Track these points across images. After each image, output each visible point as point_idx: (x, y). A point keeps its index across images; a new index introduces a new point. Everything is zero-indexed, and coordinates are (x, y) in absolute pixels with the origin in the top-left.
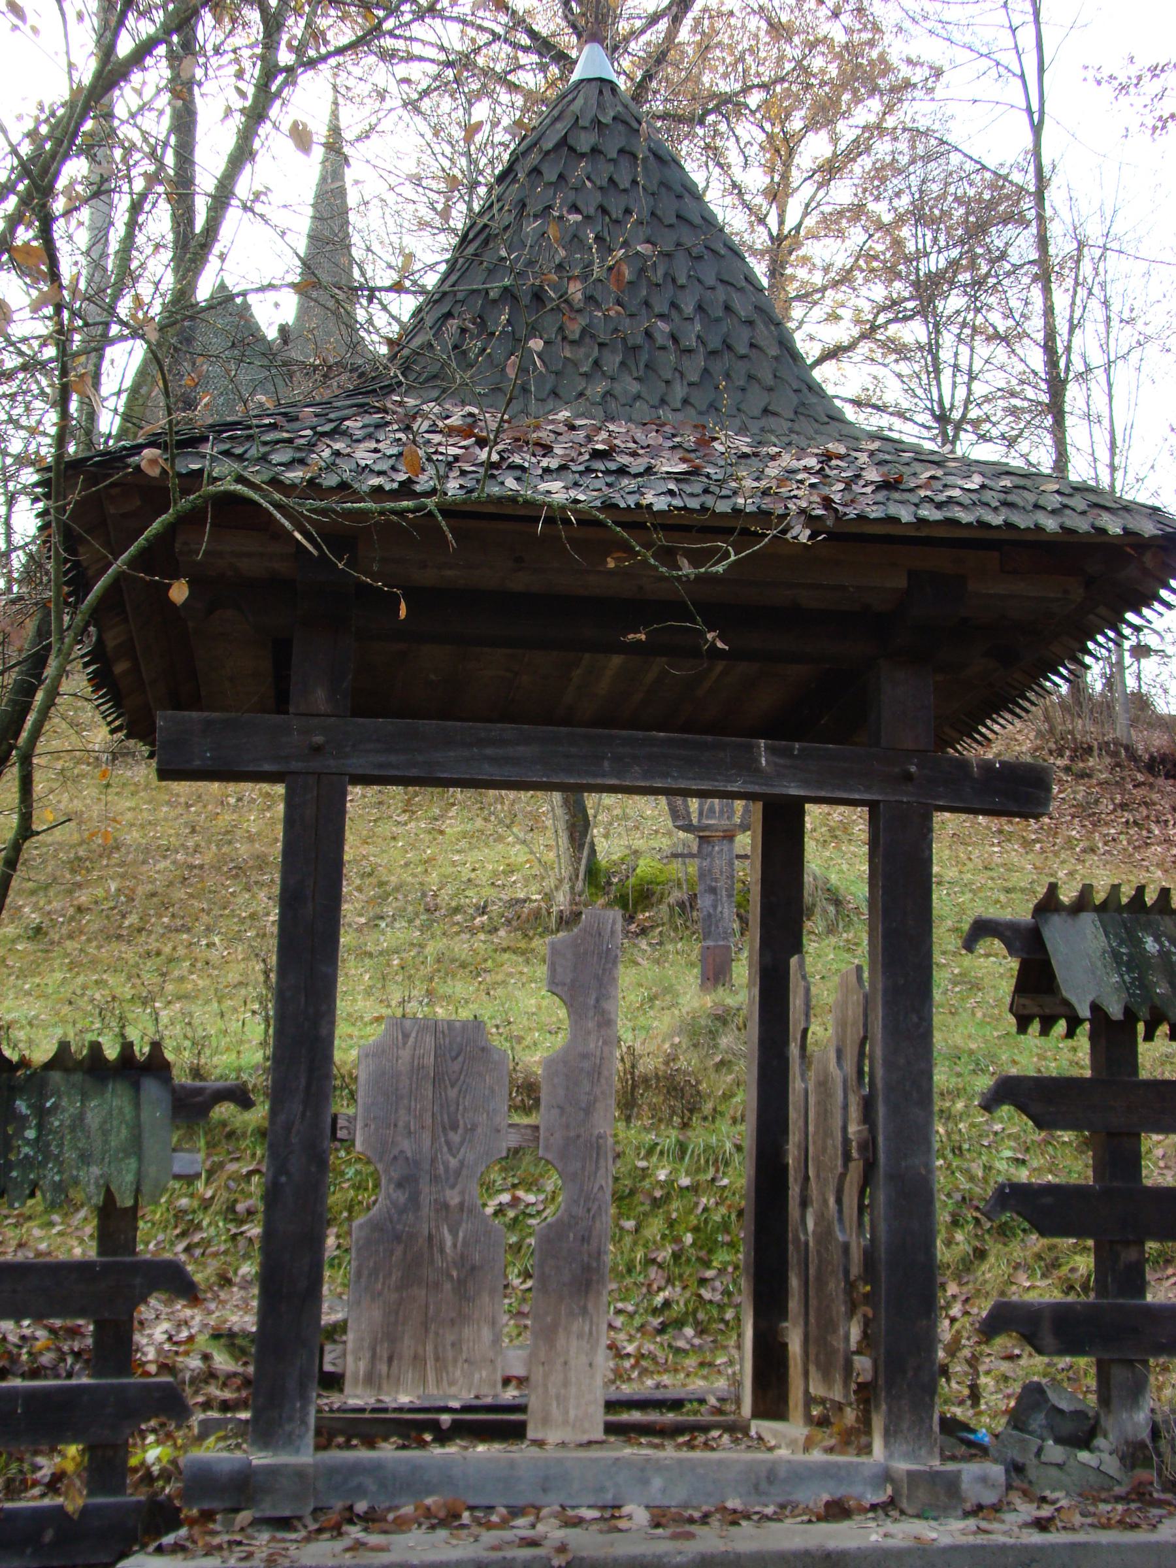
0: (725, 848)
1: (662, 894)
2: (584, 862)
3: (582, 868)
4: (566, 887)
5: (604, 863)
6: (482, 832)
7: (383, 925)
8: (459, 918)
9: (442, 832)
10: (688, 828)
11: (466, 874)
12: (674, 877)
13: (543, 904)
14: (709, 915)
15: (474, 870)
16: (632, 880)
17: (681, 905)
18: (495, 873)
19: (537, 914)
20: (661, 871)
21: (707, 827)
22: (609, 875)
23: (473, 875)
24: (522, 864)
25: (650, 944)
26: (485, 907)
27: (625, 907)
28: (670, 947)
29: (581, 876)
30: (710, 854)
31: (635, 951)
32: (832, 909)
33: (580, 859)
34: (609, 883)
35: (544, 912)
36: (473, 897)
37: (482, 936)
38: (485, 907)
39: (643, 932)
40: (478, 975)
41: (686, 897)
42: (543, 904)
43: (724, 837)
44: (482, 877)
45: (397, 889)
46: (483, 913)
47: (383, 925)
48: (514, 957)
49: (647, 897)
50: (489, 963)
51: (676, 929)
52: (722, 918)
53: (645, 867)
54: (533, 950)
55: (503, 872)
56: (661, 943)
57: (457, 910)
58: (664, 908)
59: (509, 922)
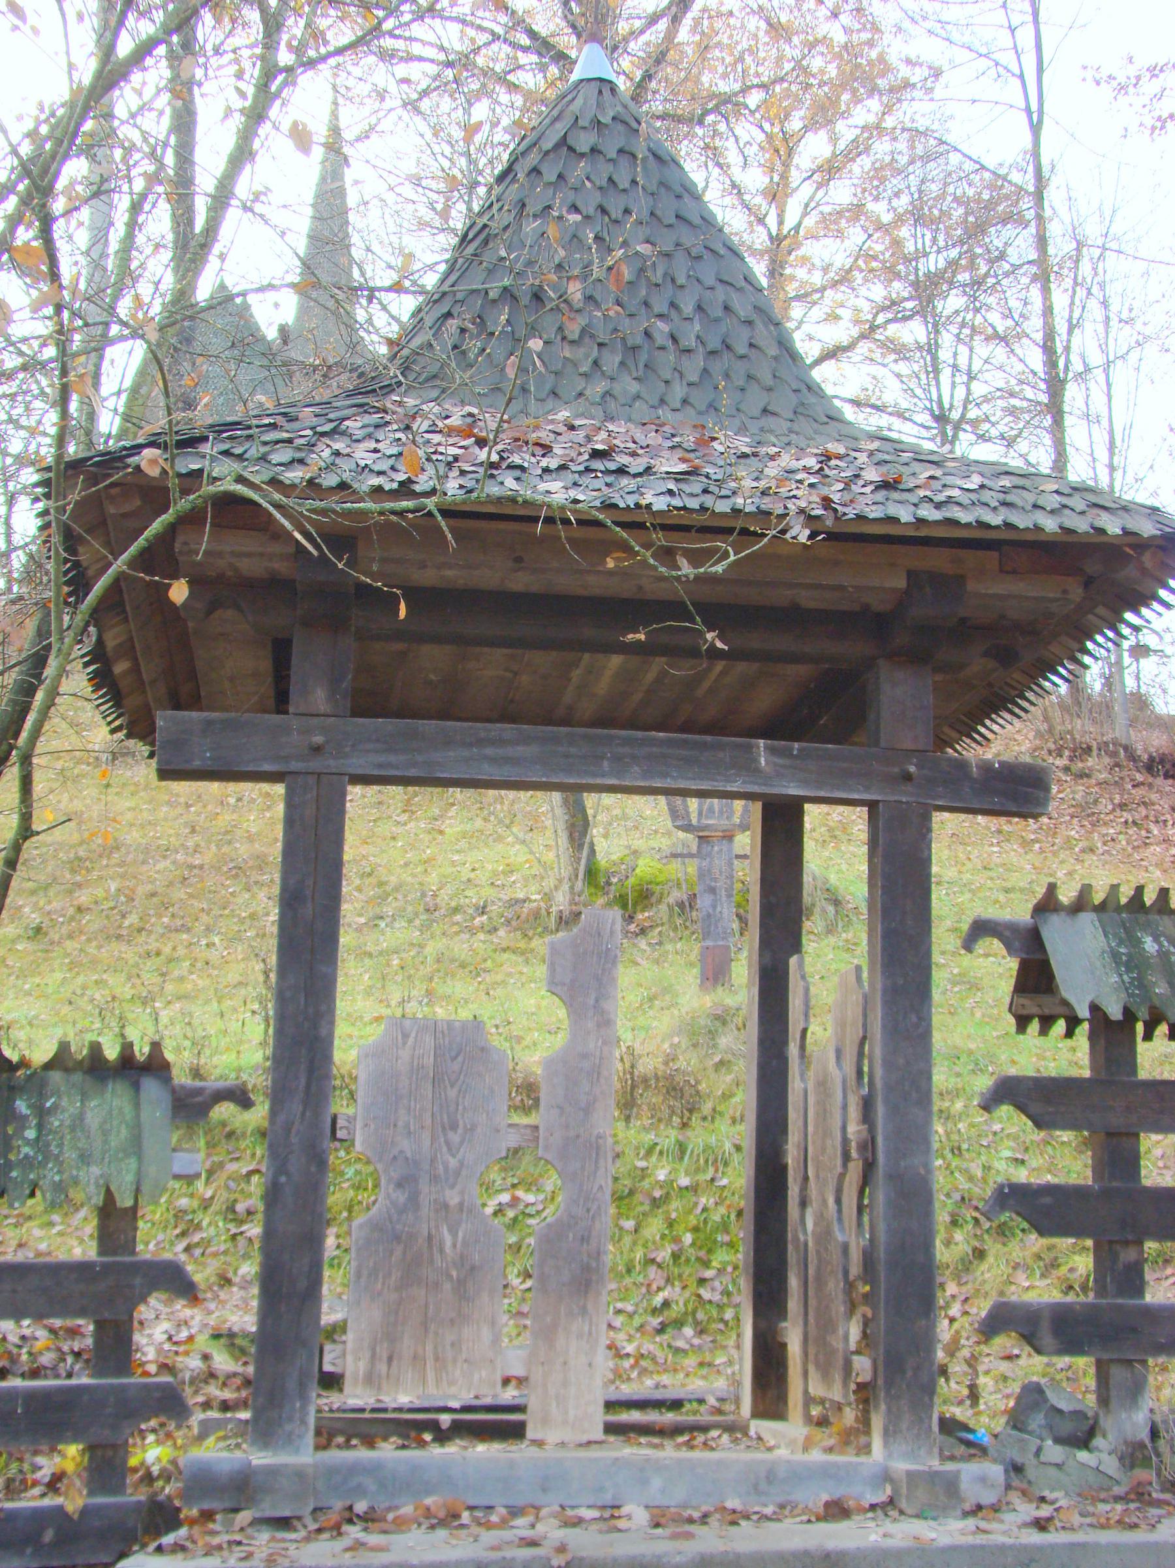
0: (725, 848)
2: (583, 862)
3: (582, 868)
4: (566, 887)
6: (481, 831)
7: (383, 925)
8: (458, 917)
9: (441, 832)
10: (688, 828)
11: (466, 874)
13: (542, 905)
14: (709, 916)
16: (632, 881)
17: (681, 905)
18: (495, 873)
19: (536, 914)
20: (660, 871)
21: (706, 827)
22: (609, 875)
23: (472, 875)
26: (484, 907)
27: (624, 906)
28: (669, 947)
29: (581, 876)
30: (709, 855)
32: (831, 909)
33: (580, 859)
34: (608, 883)
35: (543, 912)
36: (473, 897)
37: (481, 936)
38: (484, 907)
39: (643, 931)
40: (478, 975)
41: (685, 897)
44: (482, 877)
45: (396, 889)
48: (514, 957)
49: (646, 897)
50: (489, 964)
51: (676, 929)
53: (646, 867)
54: (532, 950)
55: (503, 872)
56: (660, 943)
57: (456, 910)
58: (663, 907)
59: (509, 922)
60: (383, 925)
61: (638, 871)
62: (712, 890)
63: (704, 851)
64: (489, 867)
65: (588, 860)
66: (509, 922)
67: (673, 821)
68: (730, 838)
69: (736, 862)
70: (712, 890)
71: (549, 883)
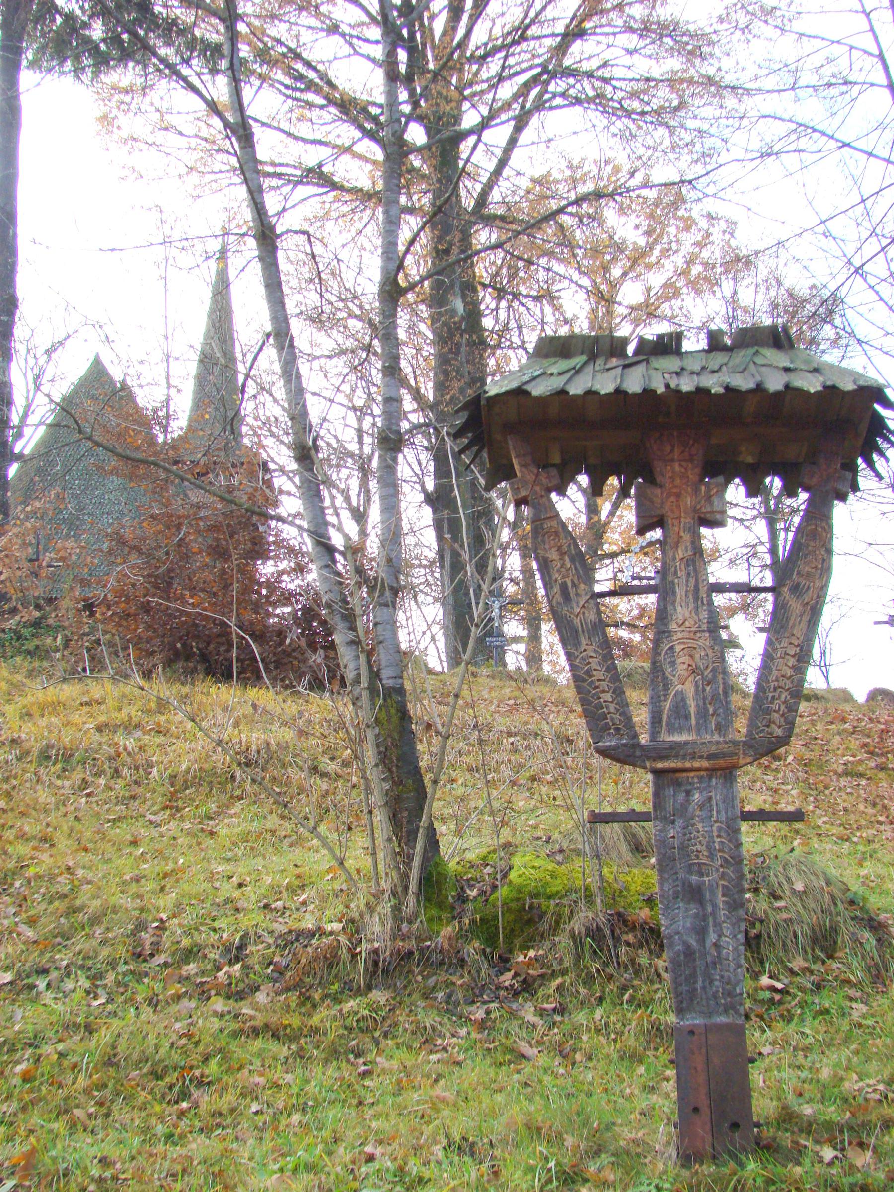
0: (717, 796)
2: (417, 862)
3: (414, 874)
4: (386, 907)
5: (452, 865)
6: (273, 832)
7: (42, 984)
8: (191, 968)
9: (212, 834)
10: (627, 755)
11: (227, 890)
12: (579, 883)
13: (343, 939)
14: (689, 953)
15: (240, 885)
16: (503, 892)
17: (595, 933)
19: (331, 959)
21: (674, 750)
22: (462, 884)
23: (236, 894)
24: (320, 876)
25: (541, 1013)
26: (241, 947)
27: (491, 940)
28: (581, 1017)
29: (413, 886)
31: (514, 1027)
32: (867, 936)
34: (462, 899)
35: (344, 954)
36: (228, 929)
37: (218, 1004)
38: (241, 947)
39: (527, 987)
40: (184, 1095)
41: (602, 919)
42: (343, 939)
43: (712, 771)
44: (251, 896)
45: (95, 921)
46: (237, 959)
50: (213, 1068)
51: (589, 980)
53: (526, 868)
56: (561, 1010)
57: (189, 954)
58: (563, 940)
60: (42, 984)
61: (513, 875)
62: (695, 894)
63: (670, 805)
64: (268, 880)
65: (425, 859)
66: (280, 972)
68: (726, 772)
69: (744, 827)
70: (695, 894)
71: (358, 904)
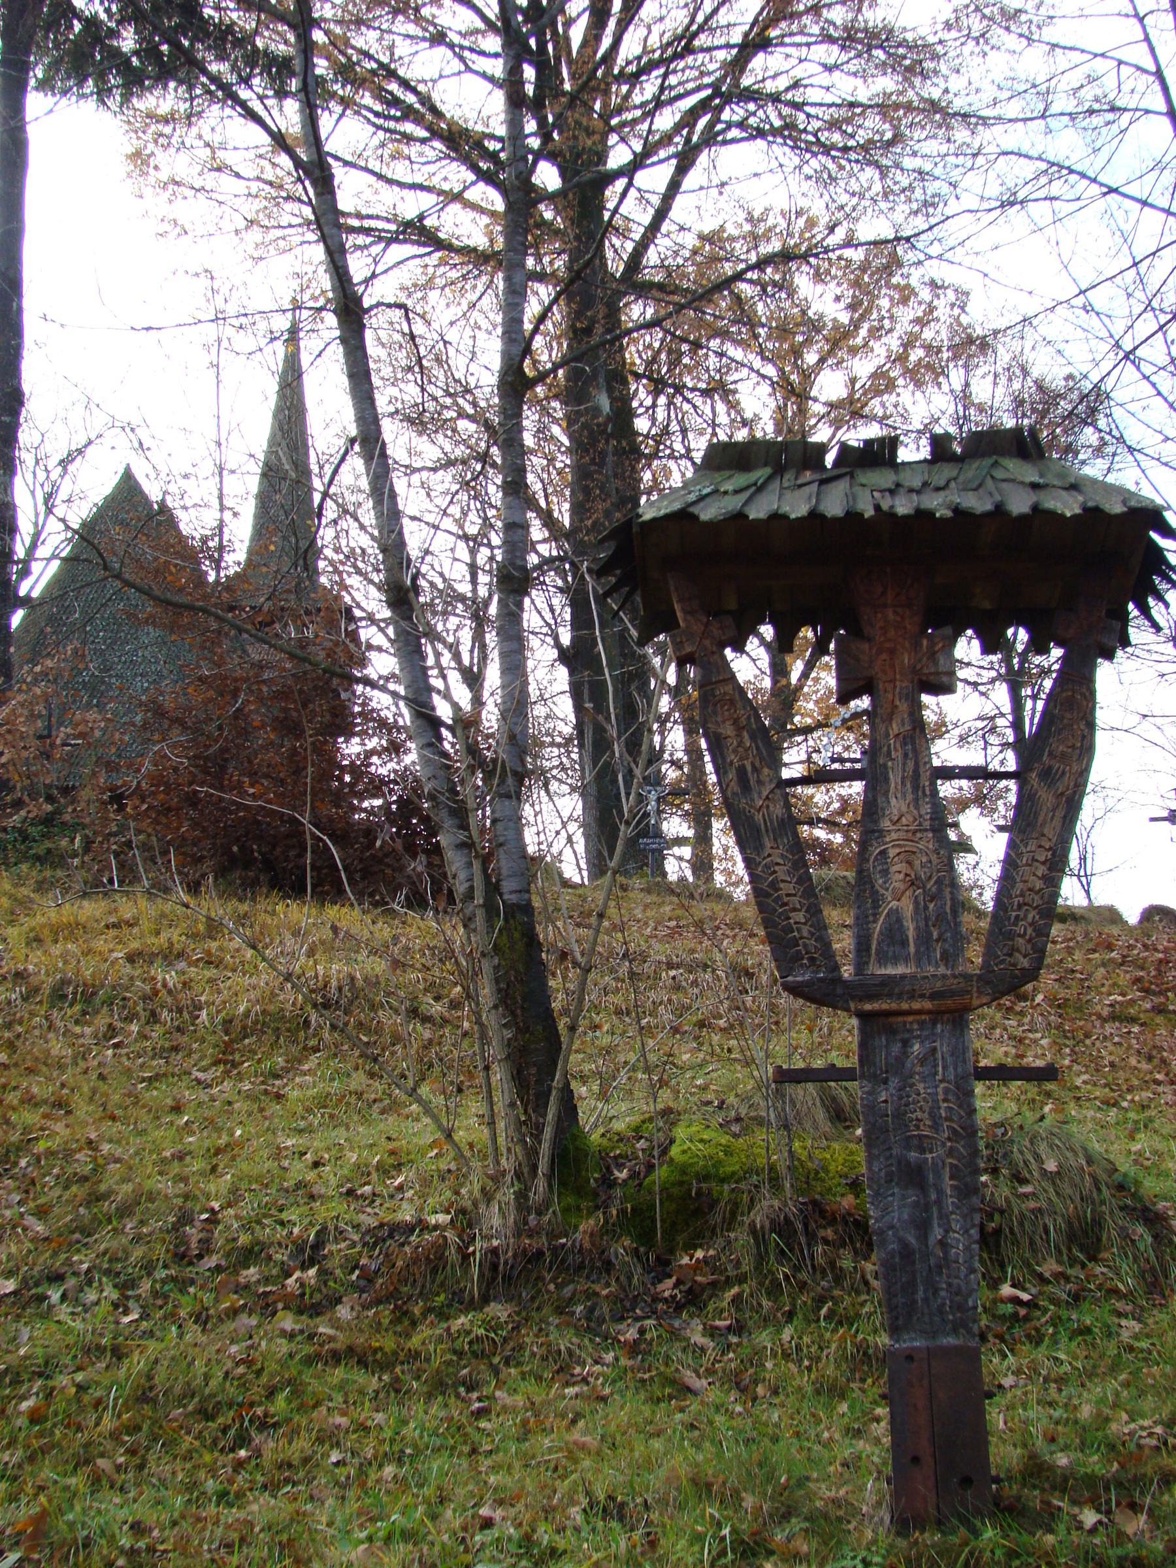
0: (943, 1047)
1: (736, 1205)
2: (548, 1133)
3: (545, 1148)
4: (507, 1194)
5: (595, 1137)
6: (359, 1095)
7: (55, 1295)
8: (251, 1273)
9: (279, 1097)
10: (825, 993)
11: (298, 1170)
14: (906, 1253)
15: (316, 1164)
16: (662, 1173)
17: (783, 1227)
18: (362, 1171)
19: (435, 1260)
20: (728, 1151)
21: (888, 986)
22: (607, 1162)
23: (311, 1176)
24: (422, 1152)
26: (318, 1245)
27: (645, 1236)
28: (764, 1338)
29: (543, 1166)
30: (898, 1066)
32: (1140, 1230)
33: (540, 1128)
34: (608, 1182)
35: (452, 1254)
36: (299, 1222)
37: (288, 1322)
38: (318, 1245)
39: (694, 1299)
43: (936, 1015)
44: (330, 1179)
45: (125, 1211)
46: (312, 1262)
47: (55, 1295)
48: (360, 1377)
49: (697, 1212)
50: (280, 1403)
51: (774, 1290)
52: (946, 1262)
53: (691, 1141)
54: (414, 1355)
55: (379, 1167)
56: (739, 1328)
57: (249, 1255)
58: (741, 1237)
59: (368, 1278)
61: (675, 1151)
62: (914, 1176)
63: (881, 1058)
64: (353, 1157)
65: (559, 1131)
66: (368, 1278)
67: (785, 971)
69: (979, 1088)
71: (471, 1188)
